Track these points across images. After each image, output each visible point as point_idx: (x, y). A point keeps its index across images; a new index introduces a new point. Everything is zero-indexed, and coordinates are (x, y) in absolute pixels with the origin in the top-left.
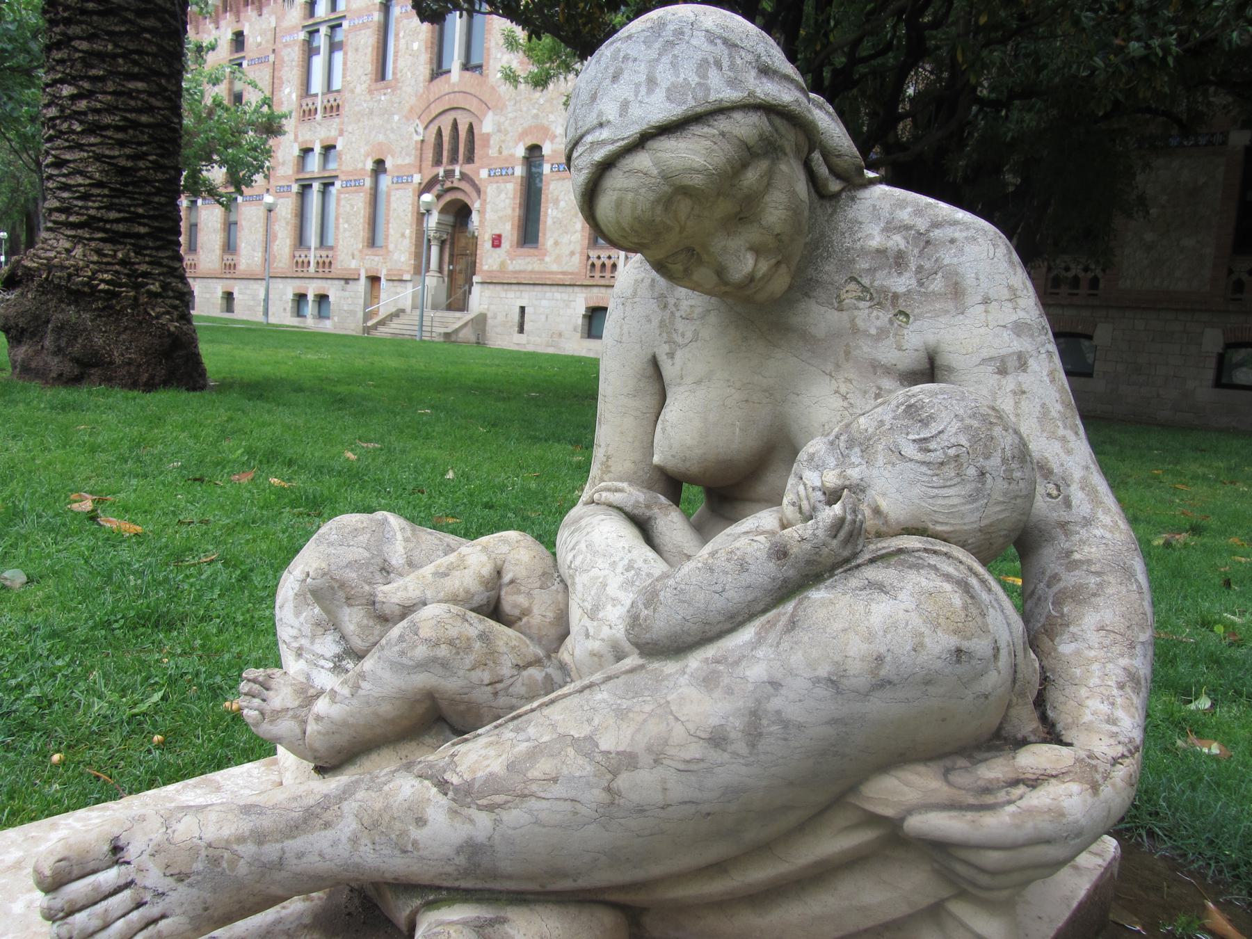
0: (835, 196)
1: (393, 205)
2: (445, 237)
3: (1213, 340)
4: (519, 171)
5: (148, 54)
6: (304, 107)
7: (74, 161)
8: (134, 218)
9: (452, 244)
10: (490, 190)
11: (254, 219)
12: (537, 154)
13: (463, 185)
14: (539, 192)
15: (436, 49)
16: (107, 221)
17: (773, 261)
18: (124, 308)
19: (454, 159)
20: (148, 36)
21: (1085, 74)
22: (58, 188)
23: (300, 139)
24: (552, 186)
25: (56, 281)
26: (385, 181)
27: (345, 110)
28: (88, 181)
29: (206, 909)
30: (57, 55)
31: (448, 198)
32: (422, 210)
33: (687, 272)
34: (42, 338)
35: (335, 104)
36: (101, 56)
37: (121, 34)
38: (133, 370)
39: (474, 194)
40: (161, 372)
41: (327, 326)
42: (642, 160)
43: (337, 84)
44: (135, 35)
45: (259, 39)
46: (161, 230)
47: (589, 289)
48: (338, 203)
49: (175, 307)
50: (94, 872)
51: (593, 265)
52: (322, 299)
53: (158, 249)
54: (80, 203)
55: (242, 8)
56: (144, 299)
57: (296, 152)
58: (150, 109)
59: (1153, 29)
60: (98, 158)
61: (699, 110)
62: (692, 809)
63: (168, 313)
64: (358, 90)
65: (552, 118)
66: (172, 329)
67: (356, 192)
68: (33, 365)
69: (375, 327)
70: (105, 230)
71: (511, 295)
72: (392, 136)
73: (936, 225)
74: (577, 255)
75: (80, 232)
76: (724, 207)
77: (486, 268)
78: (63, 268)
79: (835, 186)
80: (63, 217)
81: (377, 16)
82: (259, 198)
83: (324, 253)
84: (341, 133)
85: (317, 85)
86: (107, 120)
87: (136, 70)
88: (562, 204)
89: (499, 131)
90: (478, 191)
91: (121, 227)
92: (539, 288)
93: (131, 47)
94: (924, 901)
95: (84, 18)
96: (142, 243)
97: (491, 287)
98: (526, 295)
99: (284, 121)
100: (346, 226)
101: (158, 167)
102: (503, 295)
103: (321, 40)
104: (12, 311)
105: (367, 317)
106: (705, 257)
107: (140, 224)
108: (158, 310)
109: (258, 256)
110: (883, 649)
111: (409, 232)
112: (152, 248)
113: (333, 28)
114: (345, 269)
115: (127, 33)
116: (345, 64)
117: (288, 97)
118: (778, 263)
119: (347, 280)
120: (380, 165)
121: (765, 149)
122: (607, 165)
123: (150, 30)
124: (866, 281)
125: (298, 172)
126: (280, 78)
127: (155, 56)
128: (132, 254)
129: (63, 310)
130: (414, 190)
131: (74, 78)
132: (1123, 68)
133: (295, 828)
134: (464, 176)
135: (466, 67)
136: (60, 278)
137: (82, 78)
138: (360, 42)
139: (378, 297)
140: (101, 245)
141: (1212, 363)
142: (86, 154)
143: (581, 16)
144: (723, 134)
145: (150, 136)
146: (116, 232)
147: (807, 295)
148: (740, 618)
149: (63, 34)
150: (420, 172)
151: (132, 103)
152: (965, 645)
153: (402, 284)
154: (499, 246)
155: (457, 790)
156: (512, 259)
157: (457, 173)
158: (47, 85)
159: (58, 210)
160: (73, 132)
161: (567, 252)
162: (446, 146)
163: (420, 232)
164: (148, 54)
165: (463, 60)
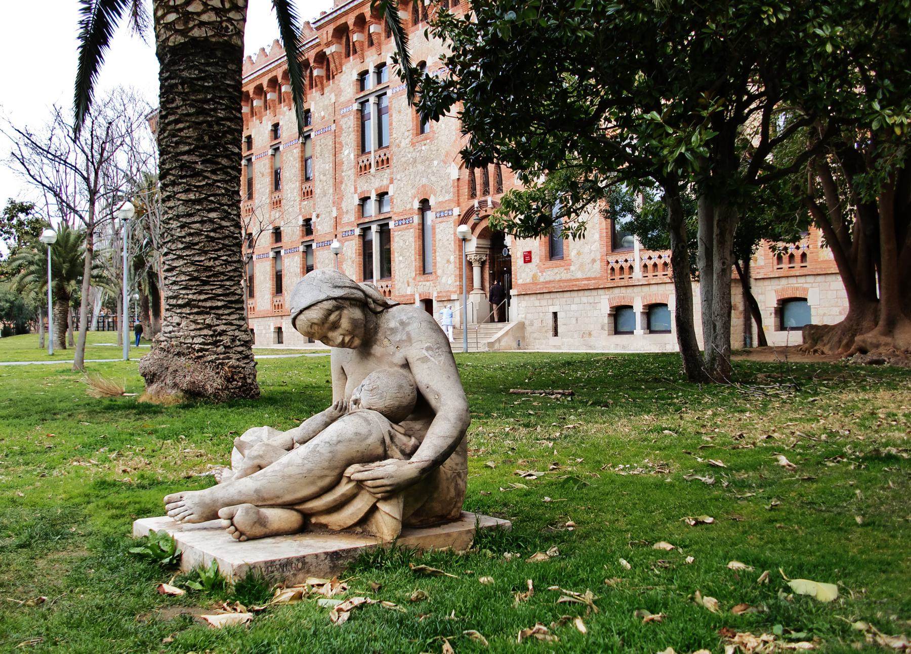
1: (438, 237)
2: (484, 258)
6: (361, 164)
8: (215, 297)
11: (327, 261)
16: (200, 301)
19: (486, 192)
22: (172, 284)
23: (359, 191)
26: (430, 216)
27: (393, 163)
28: (188, 278)
31: (484, 224)
45: (323, 114)
46: (231, 302)
47: (611, 290)
51: (613, 269)
53: (229, 314)
54: (183, 292)
57: (357, 201)
64: (403, 145)
67: (407, 228)
70: (199, 307)
71: (544, 303)
72: (433, 178)
74: (598, 262)
77: (520, 282)
84: (392, 181)
91: (208, 304)
92: (568, 294)
94: (371, 504)
96: (220, 312)
97: (527, 297)
98: (557, 302)
100: (401, 258)
102: (537, 303)
103: (371, 109)
107: (218, 300)
113: (379, 97)
114: (403, 296)
120: (425, 205)
125: (359, 218)
126: (340, 143)
130: (454, 222)
140: (197, 317)
150: (459, 206)
154: (530, 261)
156: (542, 272)
157: (489, 203)
161: (589, 261)
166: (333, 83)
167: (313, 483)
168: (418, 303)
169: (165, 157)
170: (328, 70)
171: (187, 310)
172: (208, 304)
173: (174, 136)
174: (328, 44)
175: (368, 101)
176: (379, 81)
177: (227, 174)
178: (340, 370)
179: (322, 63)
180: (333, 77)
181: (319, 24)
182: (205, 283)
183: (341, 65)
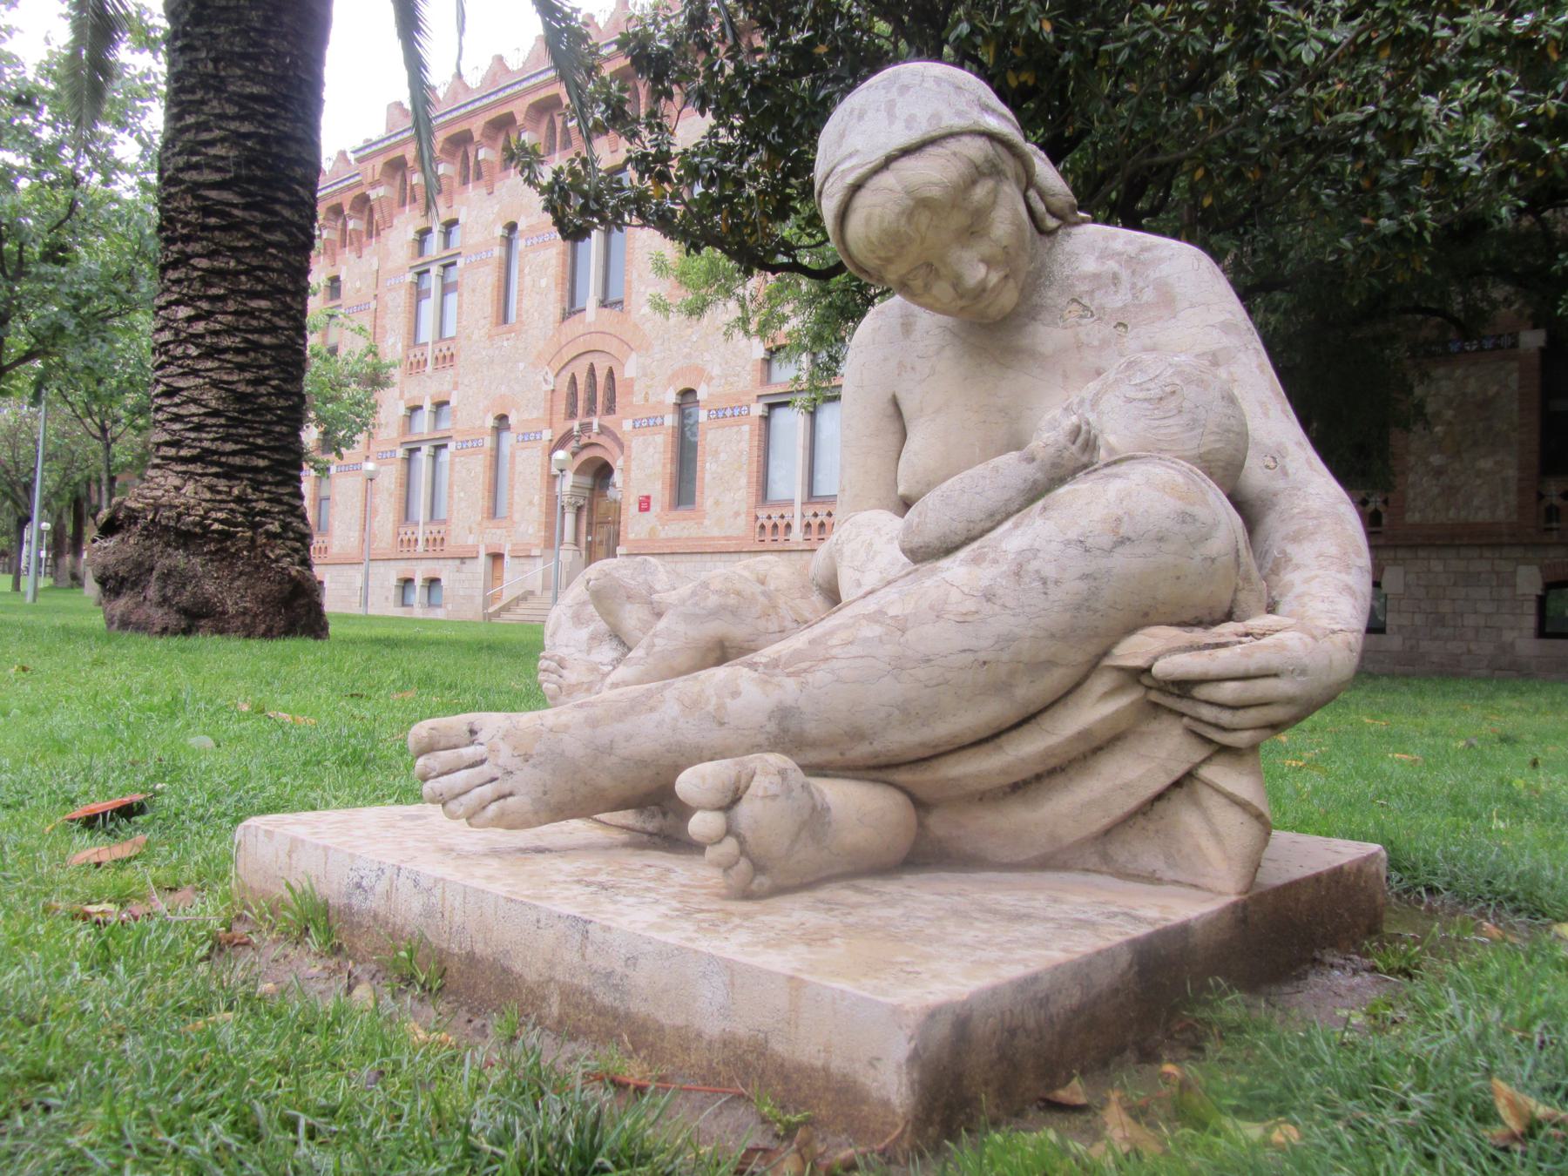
0: (1052, 233)
2: (581, 502)
3: (1529, 580)
4: (670, 420)
5: (273, 270)
7: (188, 388)
8: (253, 450)
9: (591, 510)
10: (636, 444)
12: (690, 398)
13: (602, 440)
14: (694, 447)
15: (568, 286)
17: (1002, 274)
18: (239, 550)
19: (591, 411)
20: (273, 251)
21: (1331, 259)
22: (168, 420)
23: (407, 396)
24: (710, 436)
25: (164, 522)
26: (508, 439)
27: (460, 360)
28: (202, 410)
29: (545, 793)
30: (172, 275)
31: (585, 455)
32: (555, 471)
33: (927, 287)
34: (144, 588)
35: (448, 354)
36: (222, 274)
37: (245, 249)
38: (248, 621)
39: (617, 450)
40: (280, 623)
41: (439, 614)
42: (887, 179)
43: (450, 331)
44: (258, 251)
45: (358, 284)
48: (452, 469)
49: (296, 550)
50: (456, 747)
51: (763, 527)
52: (433, 582)
53: (277, 484)
54: (193, 435)
55: (338, 251)
56: (262, 540)
57: (402, 411)
58: (272, 329)
59: (1405, 205)
60: (215, 384)
61: (934, 134)
62: (970, 657)
63: (288, 555)
64: (475, 337)
65: (707, 357)
66: (294, 573)
67: (474, 454)
68: (134, 618)
69: (498, 613)
70: (220, 464)
73: (1144, 250)
75: (191, 467)
76: (958, 220)
77: (632, 536)
78: (172, 507)
79: (1051, 223)
80: (172, 452)
81: (498, 251)
82: (357, 467)
83: (435, 529)
84: (456, 386)
85: (427, 332)
86: (226, 342)
87: (260, 287)
88: (723, 456)
89: (645, 375)
90: (621, 446)
91: (238, 461)
92: (698, 557)
93: (255, 262)
94: (1179, 770)
95: (205, 234)
96: (261, 477)
99: (392, 370)
101: (280, 392)
103: (433, 282)
104: (111, 560)
105: (487, 602)
106: (943, 271)
107: (259, 457)
108: (278, 552)
109: (355, 536)
110: (1120, 512)
111: (538, 498)
112: (271, 484)
115: (252, 248)
116: (460, 307)
117: (393, 347)
118: (1006, 277)
119: (463, 559)
121: (992, 170)
122: (857, 187)
123: (278, 245)
124: (1085, 301)
125: (404, 434)
127: (280, 272)
128: (249, 491)
129: (170, 555)
131: (192, 298)
132: (1375, 248)
133: (622, 715)
134: (603, 430)
135: (604, 304)
136: (168, 518)
137: (200, 298)
138: (478, 282)
139: (500, 578)
140: (215, 481)
141: (1531, 608)
142: (201, 381)
143: (747, 224)
144: (955, 154)
145: (273, 359)
146: (230, 466)
147: (1034, 319)
148: (998, 517)
149: (181, 252)
150: (551, 427)
151: (255, 323)
152: (1189, 509)
153: (531, 561)
154: (647, 509)
155: (766, 665)
156: (663, 525)
157: (595, 427)
158: (161, 308)
159: (168, 444)
160: (188, 357)
162: (581, 396)
163: (552, 499)
164: (273, 270)
165: (600, 296)
166: (378, 242)
167: (1001, 687)
168: (482, 557)
169: (173, 190)
170: (370, 222)
171: (197, 468)
172: (238, 461)
173: (193, 153)
174: (374, 185)
175: (428, 271)
176: (447, 245)
177: (290, 234)
178: (891, 410)
179: (361, 211)
180: (378, 234)
181: (362, 153)
182: (240, 422)
183: (391, 216)
